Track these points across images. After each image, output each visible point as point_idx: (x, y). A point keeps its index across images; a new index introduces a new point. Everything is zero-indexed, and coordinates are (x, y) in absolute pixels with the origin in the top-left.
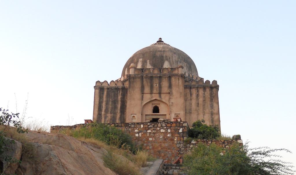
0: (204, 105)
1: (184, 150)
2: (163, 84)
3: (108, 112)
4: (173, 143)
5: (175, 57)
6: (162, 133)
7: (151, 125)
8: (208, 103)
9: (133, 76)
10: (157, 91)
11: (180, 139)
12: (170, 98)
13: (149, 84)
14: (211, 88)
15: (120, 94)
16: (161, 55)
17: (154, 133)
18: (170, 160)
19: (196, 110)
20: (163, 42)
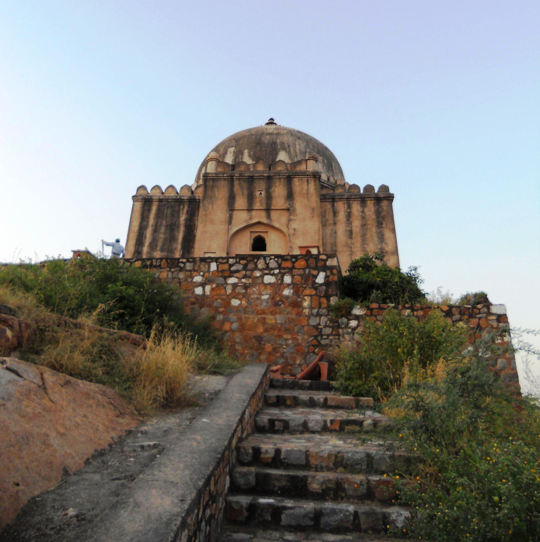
0: (364, 236)
1: (331, 334)
2: (274, 191)
3: (156, 248)
4: (299, 314)
5: (299, 144)
6: (269, 287)
7: (239, 263)
8: (373, 230)
9: (213, 175)
10: (261, 205)
11: (320, 304)
12: (290, 220)
13: (246, 192)
14: (378, 199)
15: (185, 211)
16: (273, 140)
17: (246, 287)
18: (291, 365)
19: (347, 245)
20: (275, 124)
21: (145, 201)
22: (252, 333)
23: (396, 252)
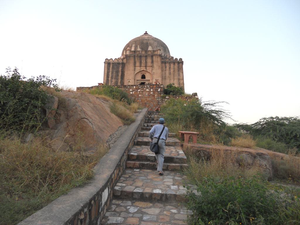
0: (174, 74)
4: (154, 98)
5: (155, 43)
8: (176, 73)
10: (144, 65)
12: (152, 70)
13: (139, 61)
14: (179, 63)
17: (142, 92)
21: (108, 63)
22: (144, 102)
23: (183, 79)
